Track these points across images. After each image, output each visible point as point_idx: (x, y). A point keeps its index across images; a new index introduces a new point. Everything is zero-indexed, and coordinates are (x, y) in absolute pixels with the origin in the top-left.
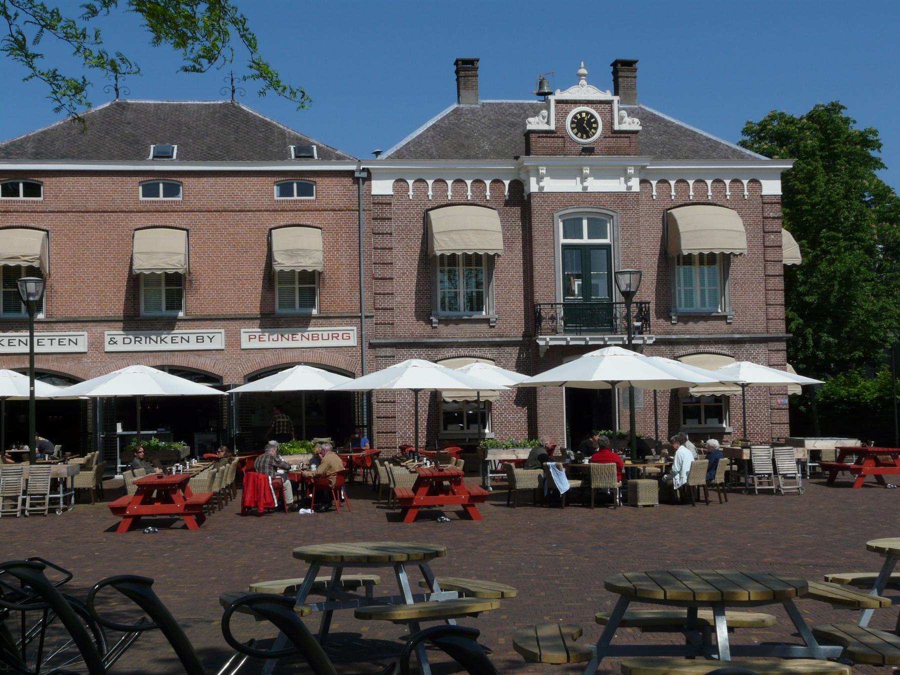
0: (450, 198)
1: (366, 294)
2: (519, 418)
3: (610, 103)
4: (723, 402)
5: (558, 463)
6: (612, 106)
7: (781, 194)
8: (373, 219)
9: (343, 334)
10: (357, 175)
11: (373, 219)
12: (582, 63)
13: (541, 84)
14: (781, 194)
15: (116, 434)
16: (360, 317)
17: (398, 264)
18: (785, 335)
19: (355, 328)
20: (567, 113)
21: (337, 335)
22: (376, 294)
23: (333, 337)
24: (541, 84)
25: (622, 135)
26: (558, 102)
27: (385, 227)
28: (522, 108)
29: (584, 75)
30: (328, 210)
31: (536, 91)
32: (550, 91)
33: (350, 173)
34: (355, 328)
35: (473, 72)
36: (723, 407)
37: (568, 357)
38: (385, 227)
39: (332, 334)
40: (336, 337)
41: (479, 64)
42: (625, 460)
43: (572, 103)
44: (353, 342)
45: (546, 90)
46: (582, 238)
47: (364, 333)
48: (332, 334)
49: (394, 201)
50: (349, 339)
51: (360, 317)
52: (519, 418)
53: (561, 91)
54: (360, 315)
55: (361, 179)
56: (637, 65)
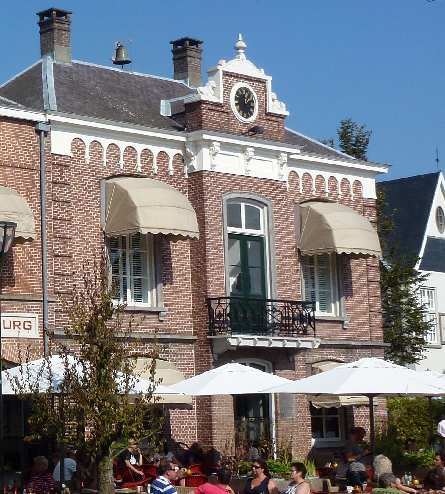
0: (122, 167)
1: (48, 275)
2: (185, 429)
3: (263, 82)
4: (339, 413)
5: (325, 479)
6: (265, 86)
7: (376, 198)
8: (52, 182)
9: (25, 322)
10: (41, 127)
11: (52, 182)
12: (240, 35)
13: (118, 51)
14: (376, 198)
15: (362, 441)
16: (43, 301)
17: (76, 240)
18: (383, 344)
19: (37, 315)
20: (231, 87)
21: (18, 323)
22: (56, 274)
23: (14, 325)
24: (118, 51)
25: (274, 118)
26: (226, 74)
27: (64, 194)
28: (118, 74)
29: (243, 48)
30: (9, 166)
31: (114, 59)
32: (128, 59)
33: (34, 123)
34: (37, 315)
35: (66, 26)
36: (339, 418)
37: (254, 359)
38: (64, 194)
39: (14, 322)
40: (18, 326)
41: (71, 17)
42: (11, 484)
43: (234, 77)
44: (35, 333)
45: (124, 57)
46: (240, 226)
47: (46, 322)
48: (14, 322)
49: (72, 166)
50: (31, 329)
51: (43, 301)
52: (185, 429)
53: (227, 62)
54: (42, 299)
55: (43, 132)
56: (201, 46)
